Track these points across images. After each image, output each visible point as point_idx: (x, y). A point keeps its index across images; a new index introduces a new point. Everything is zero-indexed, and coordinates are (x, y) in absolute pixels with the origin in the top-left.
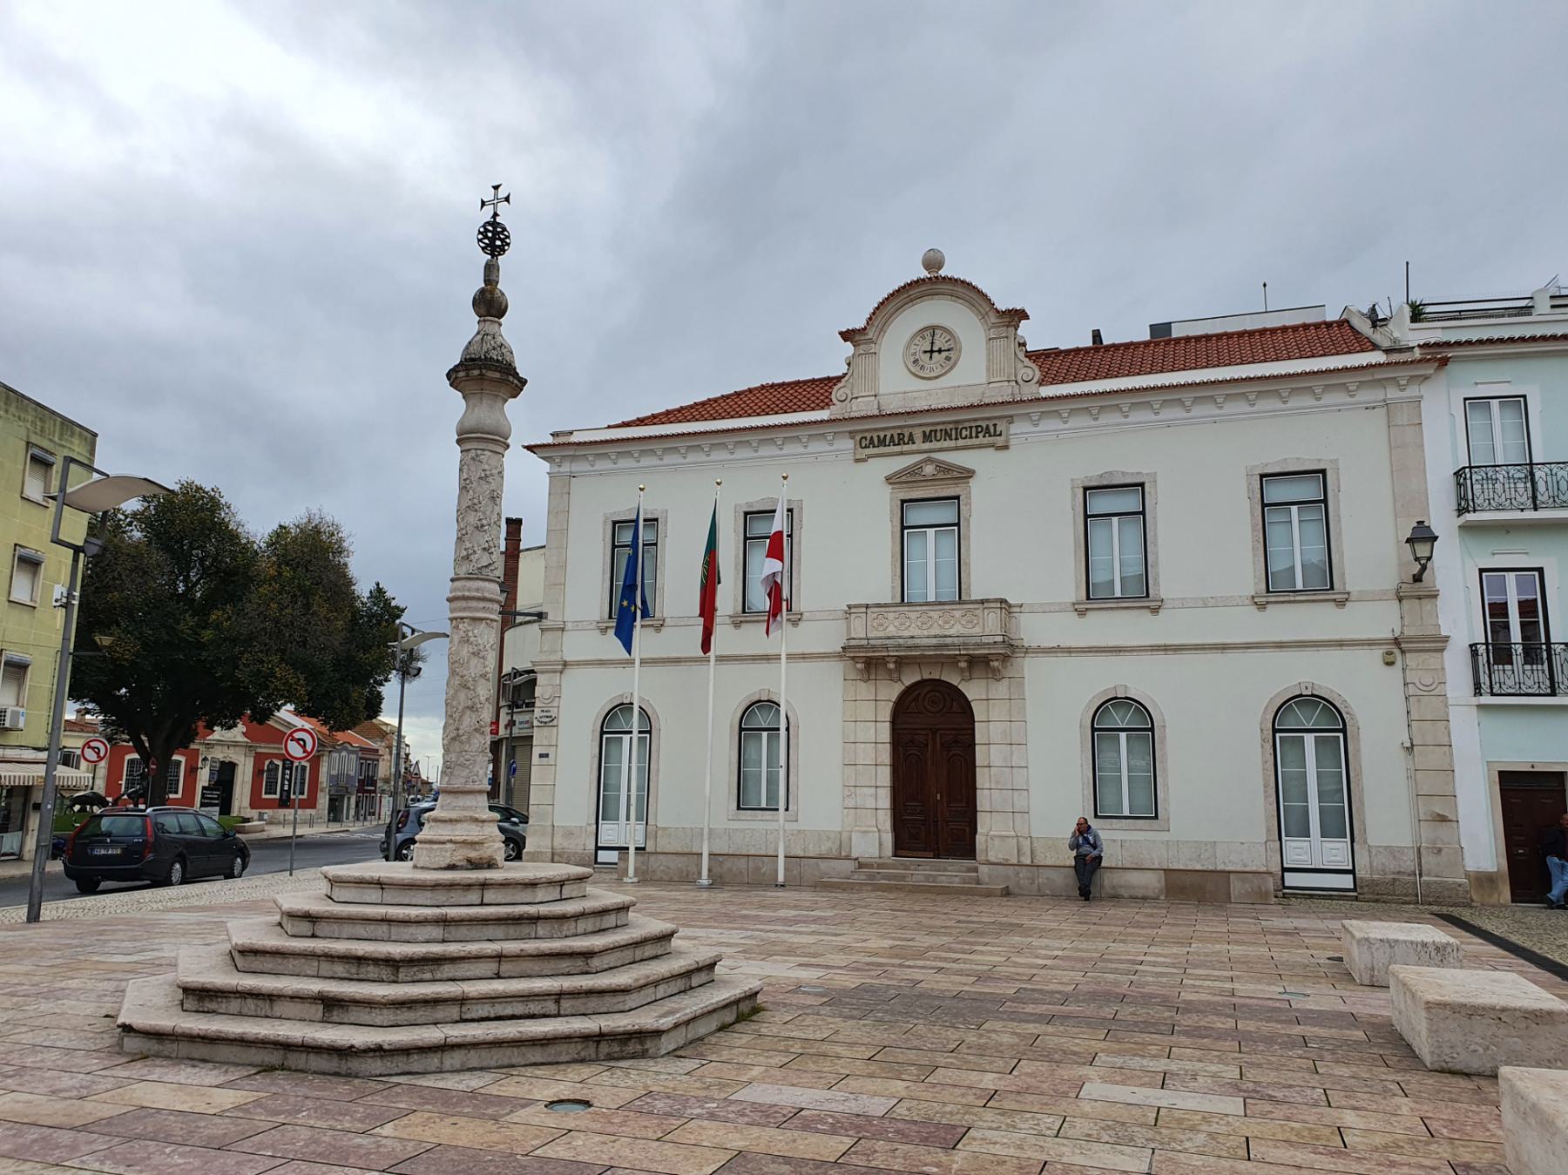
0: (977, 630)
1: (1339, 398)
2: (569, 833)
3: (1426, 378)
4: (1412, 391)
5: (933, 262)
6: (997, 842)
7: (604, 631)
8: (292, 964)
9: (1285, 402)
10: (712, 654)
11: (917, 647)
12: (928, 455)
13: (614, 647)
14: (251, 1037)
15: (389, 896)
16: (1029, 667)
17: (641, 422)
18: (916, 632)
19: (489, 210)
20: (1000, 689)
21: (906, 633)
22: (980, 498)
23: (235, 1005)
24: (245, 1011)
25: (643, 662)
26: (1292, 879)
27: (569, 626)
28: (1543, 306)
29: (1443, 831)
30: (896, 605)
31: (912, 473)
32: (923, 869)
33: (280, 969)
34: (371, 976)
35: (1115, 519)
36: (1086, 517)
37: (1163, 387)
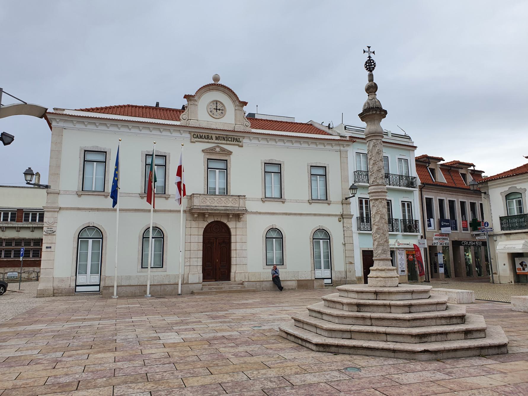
0: (237, 205)
1: (281, 144)
2: (62, 280)
3: (349, 145)
4: (346, 148)
5: (216, 79)
6: (238, 274)
7: (142, 197)
8: (427, 322)
9: (141, 131)
10: (117, 207)
11: (218, 210)
12: (219, 145)
13: (144, 204)
14: (473, 347)
15: (415, 296)
16: (248, 217)
17: (88, 110)
18: (217, 205)
19: (367, 55)
20: (240, 225)
21: (214, 205)
22: (234, 162)
23: (433, 338)
24: (437, 340)
25: (120, 210)
26: (79, 289)
27: (61, 192)
28: (390, 135)
29: (351, 265)
30: (204, 195)
31: (212, 150)
32: (213, 285)
33: (423, 324)
34: (454, 322)
35: (95, 163)
36: (85, 161)
37: (112, 119)
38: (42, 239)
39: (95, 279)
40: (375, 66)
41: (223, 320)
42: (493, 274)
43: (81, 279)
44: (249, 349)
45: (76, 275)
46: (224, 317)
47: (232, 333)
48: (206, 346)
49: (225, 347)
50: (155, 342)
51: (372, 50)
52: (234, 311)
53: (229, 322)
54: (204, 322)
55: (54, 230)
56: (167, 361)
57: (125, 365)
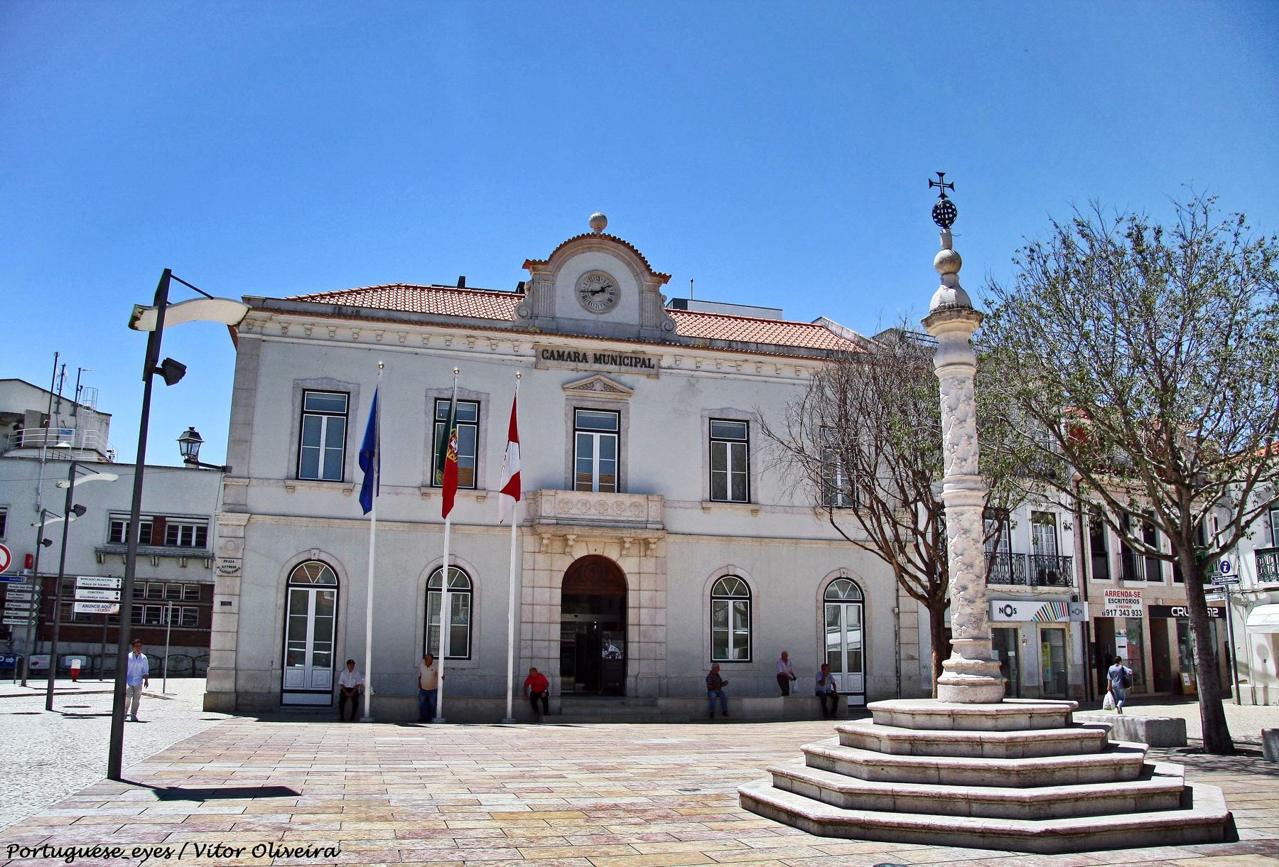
10: (373, 515)
19: (936, 191)
26: (288, 698)
38: (213, 586)
39: (322, 676)
40: (955, 215)
41: (612, 775)
42: (1237, 683)
43: (294, 675)
44: (673, 829)
45: (282, 668)
46: (613, 769)
47: (634, 800)
48: (581, 822)
49: (621, 824)
50: (472, 808)
51: (947, 180)
52: (638, 759)
53: (628, 779)
54: (570, 776)
55: (238, 564)
56: (501, 843)
57: (419, 845)
